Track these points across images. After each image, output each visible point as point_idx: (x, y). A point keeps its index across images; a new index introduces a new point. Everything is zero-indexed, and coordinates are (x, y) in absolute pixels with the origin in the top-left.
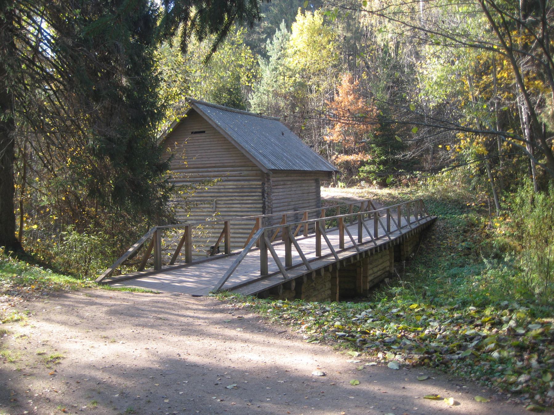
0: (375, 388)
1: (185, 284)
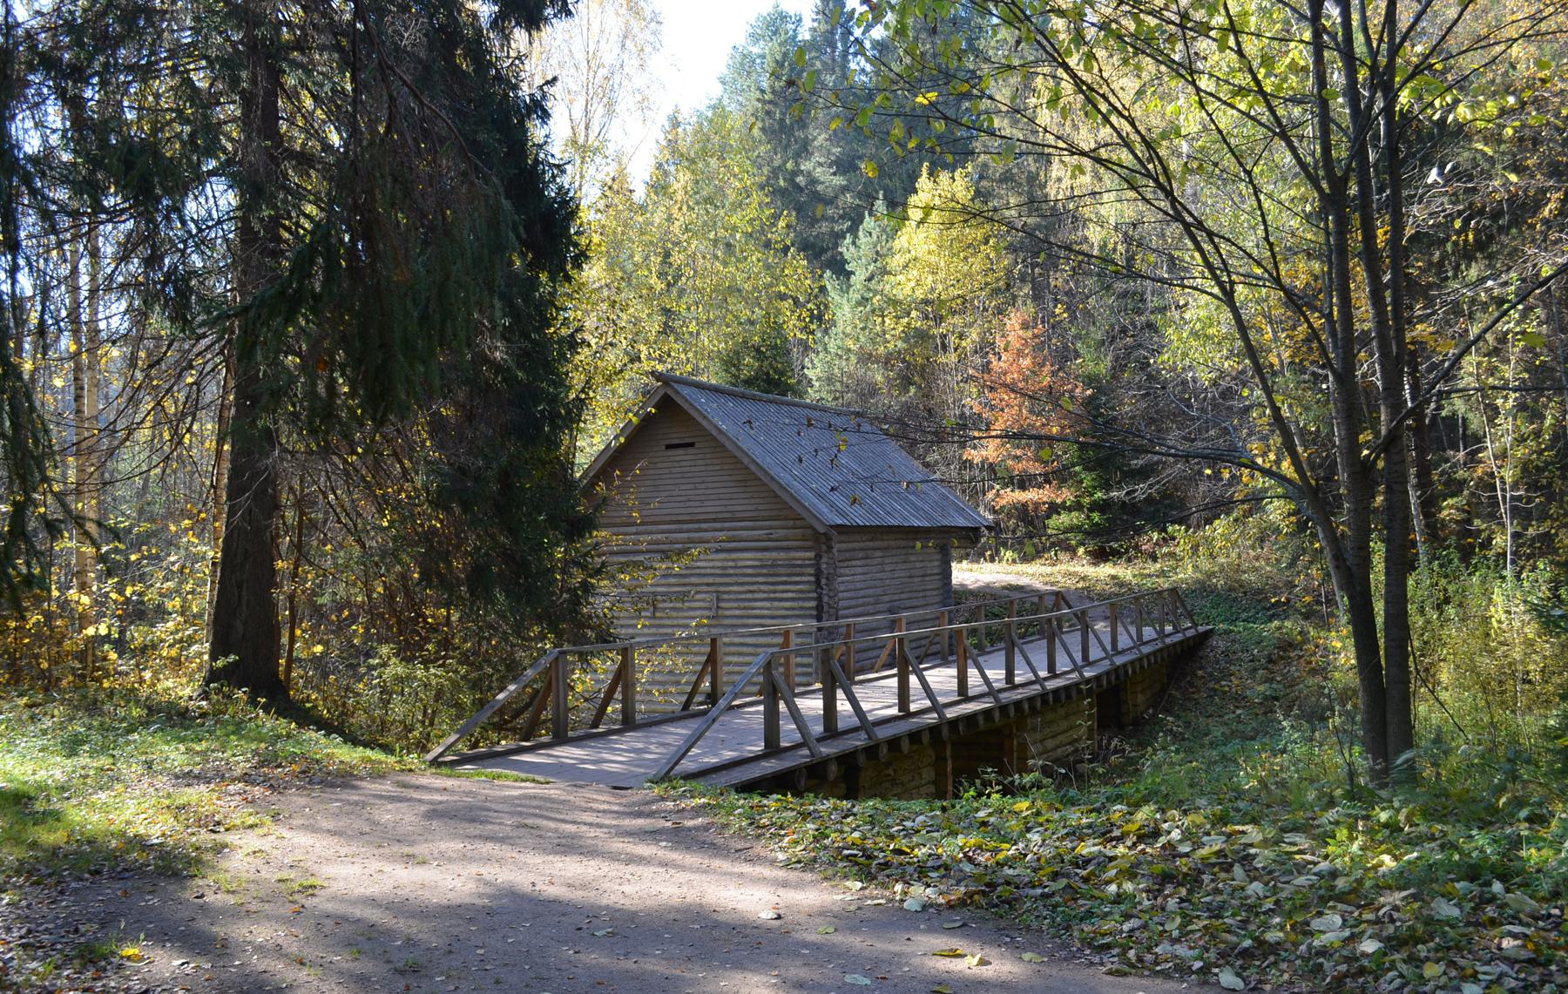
0: (856, 942)
1: (605, 766)
